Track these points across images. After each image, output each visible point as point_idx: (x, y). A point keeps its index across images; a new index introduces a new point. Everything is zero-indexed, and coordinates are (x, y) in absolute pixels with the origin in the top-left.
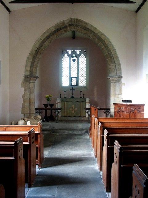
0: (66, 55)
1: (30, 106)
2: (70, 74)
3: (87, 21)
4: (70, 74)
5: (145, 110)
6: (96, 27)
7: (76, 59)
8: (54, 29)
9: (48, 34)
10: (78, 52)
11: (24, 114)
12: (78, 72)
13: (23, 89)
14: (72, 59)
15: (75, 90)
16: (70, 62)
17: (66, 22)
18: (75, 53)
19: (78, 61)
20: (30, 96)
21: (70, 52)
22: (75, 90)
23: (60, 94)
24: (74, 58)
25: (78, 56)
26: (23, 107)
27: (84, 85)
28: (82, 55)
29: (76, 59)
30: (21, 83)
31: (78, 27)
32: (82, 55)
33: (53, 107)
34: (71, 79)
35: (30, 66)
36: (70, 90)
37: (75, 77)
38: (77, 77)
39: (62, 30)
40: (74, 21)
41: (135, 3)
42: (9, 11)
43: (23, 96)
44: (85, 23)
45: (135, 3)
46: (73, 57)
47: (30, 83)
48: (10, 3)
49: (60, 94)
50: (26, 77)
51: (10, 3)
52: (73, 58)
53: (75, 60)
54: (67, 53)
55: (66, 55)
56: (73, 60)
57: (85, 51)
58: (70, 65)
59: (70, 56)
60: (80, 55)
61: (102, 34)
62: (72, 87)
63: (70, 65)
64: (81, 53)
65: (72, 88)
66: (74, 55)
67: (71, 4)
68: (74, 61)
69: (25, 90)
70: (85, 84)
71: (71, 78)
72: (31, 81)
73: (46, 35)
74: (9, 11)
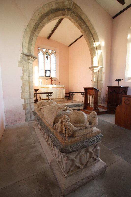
1: (29, 90)
3: (85, 11)
6: (90, 19)
7: (49, 56)
11: (25, 99)
13: (21, 69)
15: (53, 79)
16: (44, 58)
19: (50, 58)
20: (29, 79)
21: (44, 50)
23: (59, 83)
24: (47, 56)
26: (23, 91)
30: (19, 61)
33: (38, 92)
35: (28, 43)
37: (49, 70)
39: (61, 12)
40: (73, 6)
44: (82, 12)
47: (28, 63)
49: (59, 83)
53: (48, 57)
54: (42, 51)
56: (46, 57)
64: (52, 52)
66: (47, 53)
68: (47, 58)
72: (30, 61)
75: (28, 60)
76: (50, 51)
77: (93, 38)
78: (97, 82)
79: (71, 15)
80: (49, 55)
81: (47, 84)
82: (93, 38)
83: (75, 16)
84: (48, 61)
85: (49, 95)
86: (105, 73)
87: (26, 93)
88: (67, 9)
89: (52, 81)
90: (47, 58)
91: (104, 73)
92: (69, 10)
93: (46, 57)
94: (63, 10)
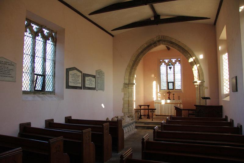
0: (163, 64)
2: (167, 80)
4: (167, 80)
5: (50, 119)
8: (146, 46)
9: (141, 49)
10: (174, 61)
12: (174, 77)
13: (123, 93)
14: (168, 67)
15: (171, 93)
16: (167, 68)
17: (155, 39)
18: (170, 61)
19: (174, 68)
21: (167, 61)
22: (171, 93)
23: (179, 97)
24: (170, 66)
25: (174, 64)
26: (123, 108)
27: (179, 89)
28: (177, 63)
29: (172, 67)
31: (165, 42)
32: (177, 63)
34: (168, 84)
36: (168, 93)
37: (171, 82)
38: (173, 82)
41: (210, 18)
42: (113, 36)
43: (123, 99)
45: (210, 18)
46: (169, 65)
47: (128, 88)
48: (111, 31)
49: (179, 97)
50: (125, 84)
51: (111, 31)
52: (169, 66)
54: (165, 62)
55: (163, 64)
57: (179, 59)
58: (167, 72)
59: (167, 65)
60: (175, 63)
61: (186, 46)
62: (169, 90)
63: (167, 72)
65: (169, 91)
67: (155, 26)
68: (170, 68)
69: (124, 94)
70: (180, 87)
71: (168, 83)
72: (129, 87)
73: (140, 51)
74: (113, 36)
75: (128, 86)
76: (174, 61)
77: (189, 54)
78: (199, 98)
79: (162, 43)
80: (172, 65)
81: (174, 99)
82: (189, 54)
83: (166, 43)
84: (171, 72)
85: (152, 111)
86: (208, 88)
87: (126, 109)
88: (158, 41)
89: (169, 95)
90: (170, 68)
91: (207, 88)
92: (159, 41)
93: (169, 67)
94: (155, 43)
